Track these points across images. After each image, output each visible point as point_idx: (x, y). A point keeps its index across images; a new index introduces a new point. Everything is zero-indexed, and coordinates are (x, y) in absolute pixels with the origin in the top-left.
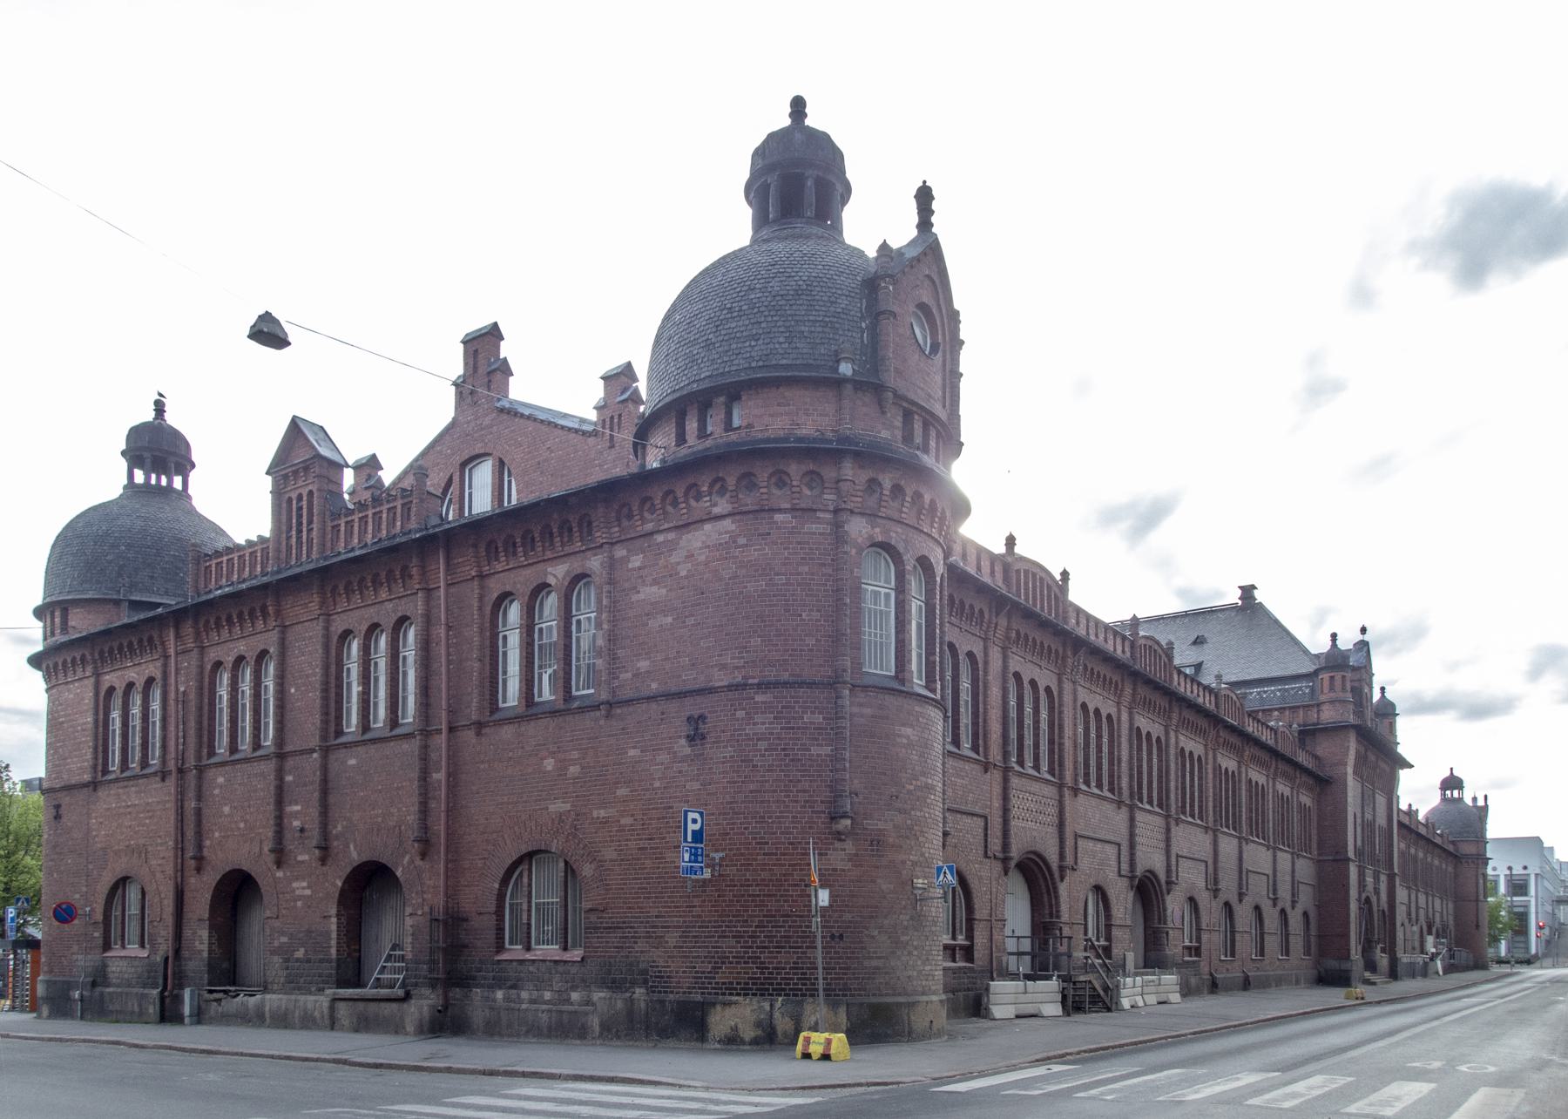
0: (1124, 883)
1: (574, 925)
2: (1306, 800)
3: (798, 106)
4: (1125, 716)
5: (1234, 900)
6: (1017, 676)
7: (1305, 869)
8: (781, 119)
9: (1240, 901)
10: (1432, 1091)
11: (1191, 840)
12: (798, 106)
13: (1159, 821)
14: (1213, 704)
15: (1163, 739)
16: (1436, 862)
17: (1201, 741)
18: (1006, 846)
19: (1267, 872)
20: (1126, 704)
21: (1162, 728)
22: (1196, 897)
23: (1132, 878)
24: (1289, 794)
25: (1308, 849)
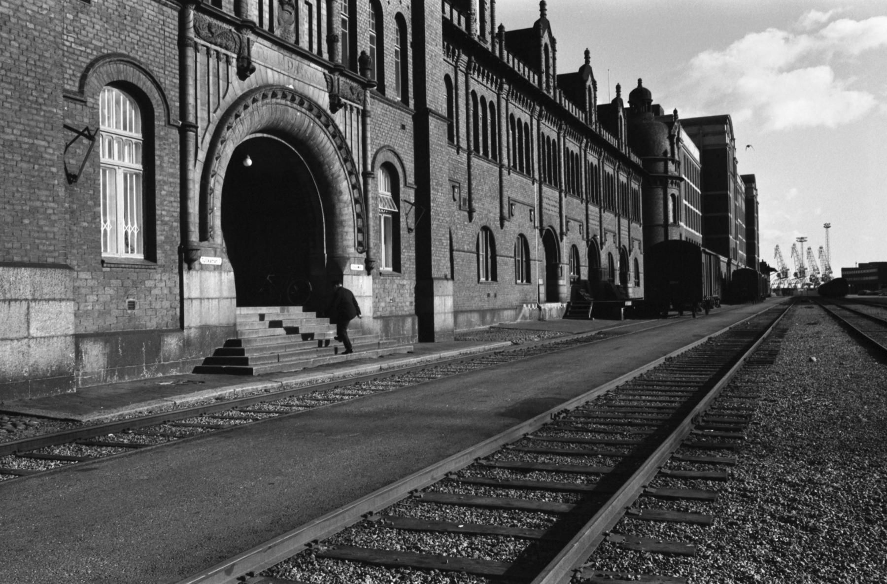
0: (584, 243)
1: (110, 204)
2: (635, 186)
3: (640, 81)
4: (461, 78)
5: (494, 225)
6: (474, 93)
7: (638, 231)
8: (636, 86)
9: (502, 226)
10: (791, 299)
11: (574, 206)
12: (640, 81)
13: (597, 210)
14: (536, 81)
15: (556, 140)
16: (623, 178)
17: (527, 111)
18: (588, 233)
19: (613, 229)
20: (536, 117)
21: (495, 95)
22: (525, 233)
23: (541, 231)
24: (495, 100)
25: (637, 220)
